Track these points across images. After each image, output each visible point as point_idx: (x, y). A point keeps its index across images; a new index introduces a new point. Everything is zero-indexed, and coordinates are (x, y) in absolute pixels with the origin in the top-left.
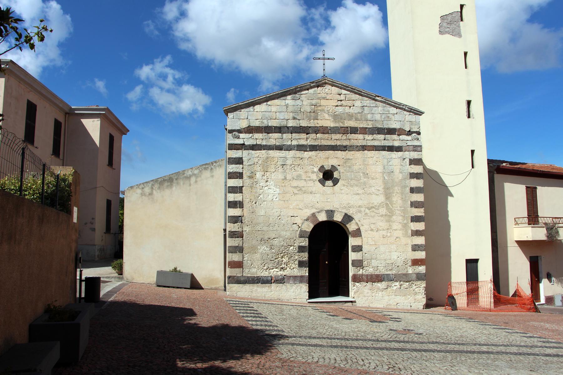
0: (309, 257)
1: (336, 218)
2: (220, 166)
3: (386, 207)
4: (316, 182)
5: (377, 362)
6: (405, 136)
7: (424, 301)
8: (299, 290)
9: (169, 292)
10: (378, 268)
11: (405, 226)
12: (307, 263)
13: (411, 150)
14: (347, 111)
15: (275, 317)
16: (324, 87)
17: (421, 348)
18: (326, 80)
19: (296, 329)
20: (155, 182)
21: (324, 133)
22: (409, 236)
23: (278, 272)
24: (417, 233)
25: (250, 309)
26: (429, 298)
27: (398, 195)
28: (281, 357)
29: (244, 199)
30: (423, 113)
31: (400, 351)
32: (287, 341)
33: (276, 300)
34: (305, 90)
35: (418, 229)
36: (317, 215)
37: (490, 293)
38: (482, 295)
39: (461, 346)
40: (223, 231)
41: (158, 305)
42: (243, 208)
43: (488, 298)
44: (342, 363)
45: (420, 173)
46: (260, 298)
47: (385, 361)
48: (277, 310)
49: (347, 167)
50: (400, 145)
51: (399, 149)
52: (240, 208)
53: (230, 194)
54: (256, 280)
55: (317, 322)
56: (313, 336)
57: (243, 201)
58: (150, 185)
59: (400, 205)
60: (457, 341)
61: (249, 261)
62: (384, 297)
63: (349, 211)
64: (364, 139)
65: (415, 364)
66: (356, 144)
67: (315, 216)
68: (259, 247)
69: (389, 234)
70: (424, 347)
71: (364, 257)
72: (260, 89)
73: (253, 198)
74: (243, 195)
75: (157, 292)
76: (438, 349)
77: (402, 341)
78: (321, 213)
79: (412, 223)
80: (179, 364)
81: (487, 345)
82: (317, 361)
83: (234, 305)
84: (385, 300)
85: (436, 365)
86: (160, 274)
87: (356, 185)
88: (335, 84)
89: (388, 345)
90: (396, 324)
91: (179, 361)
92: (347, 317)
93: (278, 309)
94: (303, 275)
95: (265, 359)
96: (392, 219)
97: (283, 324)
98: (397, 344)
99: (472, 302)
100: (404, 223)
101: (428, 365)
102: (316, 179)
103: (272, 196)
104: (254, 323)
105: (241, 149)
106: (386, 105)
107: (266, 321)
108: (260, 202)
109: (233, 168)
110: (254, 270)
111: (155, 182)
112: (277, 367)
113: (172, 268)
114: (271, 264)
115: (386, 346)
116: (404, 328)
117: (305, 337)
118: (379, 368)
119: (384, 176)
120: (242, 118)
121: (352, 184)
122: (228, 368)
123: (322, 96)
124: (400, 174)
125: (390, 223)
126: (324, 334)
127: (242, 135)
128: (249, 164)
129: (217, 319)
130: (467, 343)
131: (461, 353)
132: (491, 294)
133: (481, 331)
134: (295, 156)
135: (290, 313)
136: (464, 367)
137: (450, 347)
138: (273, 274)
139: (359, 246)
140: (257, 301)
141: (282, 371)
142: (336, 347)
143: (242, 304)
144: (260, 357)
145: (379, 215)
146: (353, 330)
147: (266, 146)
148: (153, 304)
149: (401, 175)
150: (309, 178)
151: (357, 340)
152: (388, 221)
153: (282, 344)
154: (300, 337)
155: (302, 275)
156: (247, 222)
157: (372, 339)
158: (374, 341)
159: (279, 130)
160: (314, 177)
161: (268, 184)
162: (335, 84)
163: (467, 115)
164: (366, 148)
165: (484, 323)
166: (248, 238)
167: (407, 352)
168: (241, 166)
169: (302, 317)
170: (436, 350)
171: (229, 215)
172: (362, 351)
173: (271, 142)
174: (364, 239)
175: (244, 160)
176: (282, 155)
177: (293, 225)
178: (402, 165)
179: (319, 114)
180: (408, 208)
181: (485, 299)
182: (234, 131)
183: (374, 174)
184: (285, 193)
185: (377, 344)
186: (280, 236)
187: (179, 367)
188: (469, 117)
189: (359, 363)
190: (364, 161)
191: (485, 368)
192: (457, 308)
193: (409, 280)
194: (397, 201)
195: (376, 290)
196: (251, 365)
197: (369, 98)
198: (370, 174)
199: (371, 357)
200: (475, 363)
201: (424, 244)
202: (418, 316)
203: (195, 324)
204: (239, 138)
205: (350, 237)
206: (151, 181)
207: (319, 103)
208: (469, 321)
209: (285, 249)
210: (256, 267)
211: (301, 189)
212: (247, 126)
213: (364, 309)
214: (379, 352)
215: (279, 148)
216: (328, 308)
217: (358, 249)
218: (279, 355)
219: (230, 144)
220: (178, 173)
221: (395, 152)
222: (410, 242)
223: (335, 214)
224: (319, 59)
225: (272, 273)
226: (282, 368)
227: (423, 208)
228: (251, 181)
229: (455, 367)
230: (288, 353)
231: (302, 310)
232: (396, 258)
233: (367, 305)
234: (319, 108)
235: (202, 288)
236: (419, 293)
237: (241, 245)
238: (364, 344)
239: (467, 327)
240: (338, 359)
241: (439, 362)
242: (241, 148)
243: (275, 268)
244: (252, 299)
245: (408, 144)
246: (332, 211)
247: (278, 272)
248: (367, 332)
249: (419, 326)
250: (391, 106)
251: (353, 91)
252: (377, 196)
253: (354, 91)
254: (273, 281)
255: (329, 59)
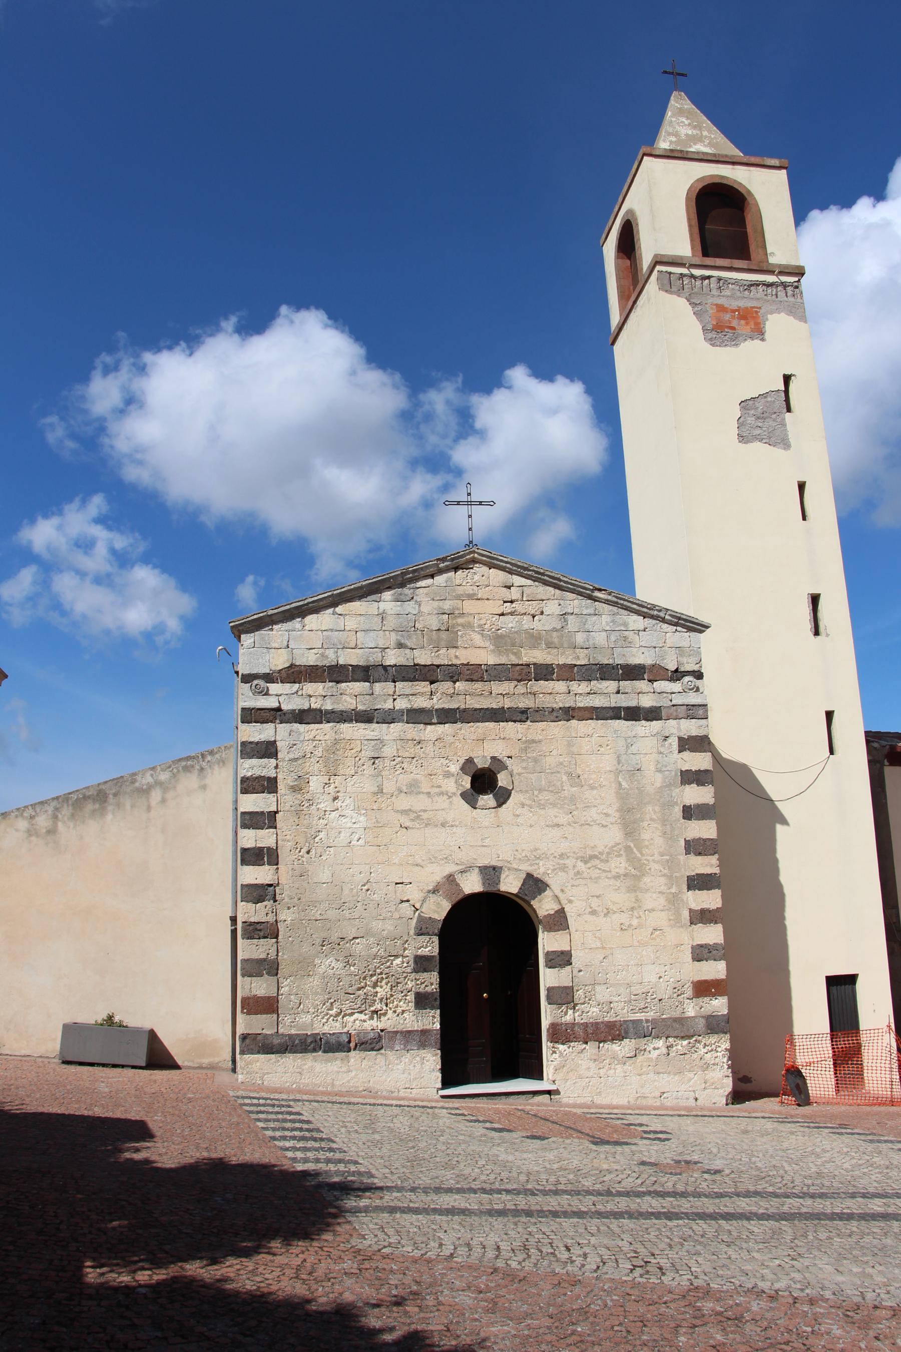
0: (442, 984)
1: (505, 884)
2: (222, 762)
3: (627, 856)
4: (454, 797)
5: (603, 1251)
6: (667, 682)
7: (728, 1085)
8: (418, 1066)
9: (91, 1079)
10: (612, 1005)
11: (674, 900)
12: (436, 999)
13: (681, 716)
14: (526, 627)
15: (354, 1139)
16: (471, 570)
17: (717, 1211)
18: (474, 552)
19: (405, 1170)
20: (63, 801)
21: (472, 681)
22: (685, 924)
23: (365, 1021)
24: (702, 917)
25: (292, 1117)
26: (740, 1076)
27: (655, 825)
28: (360, 1247)
29: (279, 842)
30: (707, 627)
31: (665, 1221)
32: (377, 1201)
33: (361, 1091)
34: (426, 577)
35: (705, 906)
36: (458, 877)
37: (889, 1059)
38: (870, 1064)
39: (818, 1200)
40: (230, 922)
41: (58, 1114)
42: (277, 864)
43: (884, 1072)
44: (515, 1258)
45: (706, 771)
46: (321, 1088)
47: (623, 1249)
48: (359, 1118)
49: (530, 760)
50: (655, 704)
51: (653, 714)
52: (269, 864)
53: (246, 831)
54: (311, 1042)
55: (459, 1150)
56: (445, 1186)
57: (277, 847)
58: (50, 809)
59: (661, 850)
60: (808, 1189)
61: (292, 997)
62: (628, 1078)
63: (536, 867)
64: (569, 693)
65: (700, 1254)
66: (548, 706)
67: (454, 880)
68: (317, 961)
69: (635, 922)
70: (726, 1206)
71: (576, 980)
72: (316, 574)
73: (301, 840)
74: (277, 834)
75: (61, 1079)
76: (761, 1211)
77: (669, 1192)
78: (468, 874)
79: (690, 892)
80: (90, 1276)
81: (883, 1195)
82: (452, 1254)
83: (252, 1108)
84: (631, 1084)
85: (755, 1254)
86: (71, 1031)
87: (551, 804)
88: (496, 562)
89: (633, 1204)
90: (656, 1146)
91: (92, 1267)
92: (535, 1134)
93: (364, 1116)
94: (428, 1027)
95: (317, 1254)
96: (642, 885)
97: (372, 1157)
98: (657, 1201)
99: (845, 1084)
100: (671, 893)
101: (733, 1257)
102: (454, 790)
103: (348, 834)
104: (299, 1155)
105: (271, 722)
106: (620, 610)
107: (331, 1150)
108: (319, 850)
109: (254, 767)
110: (306, 1019)
111: (63, 801)
112: (346, 1273)
113: (101, 1016)
114: (348, 1002)
115: (628, 1206)
116: (675, 1158)
117: (426, 1190)
118: (609, 1268)
119: (620, 779)
120: (276, 645)
121: (542, 802)
122: (219, 1281)
123: (467, 592)
124: (657, 774)
125: (638, 893)
126: (474, 1180)
127: (274, 688)
128: (291, 756)
129: (205, 1146)
130: (833, 1193)
131: (816, 1219)
132: (890, 1061)
133: (869, 1158)
134: (403, 737)
135: (392, 1125)
136: (826, 1259)
137: (790, 1204)
138: (353, 1028)
139: (562, 952)
140: (311, 1097)
141: (359, 1285)
142: (502, 1213)
143: (273, 1106)
144: (304, 1249)
145: (609, 875)
146: (548, 1166)
147: (333, 712)
148: (45, 1110)
149: (659, 776)
150: (437, 790)
151: (556, 1192)
152: (632, 889)
153: (366, 1210)
154: (413, 1190)
155: (425, 1027)
156: (286, 900)
157: (593, 1190)
158: (599, 1193)
159: (364, 673)
160: (450, 785)
161: (340, 804)
162: (496, 562)
163: (813, 630)
164: (575, 714)
165: (876, 1138)
166: (290, 939)
167: (681, 1222)
168: (273, 762)
169: (422, 1136)
170: (756, 1214)
171: (244, 883)
172: (567, 1223)
173: (345, 704)
174: (576, 936)
175: (279, 749)
176: (372, 733)
177: (400, 905)
178: (661, 753)
179: (459, 633)
180: (679, 857)
181: (878, 1075)
182: (255, 676)
183: (593, 776)
184: (379, 825)
185: (607, 1202)
186: (368, 933)
187: (90, 1286)
188: (817, 633)
189: (558, 1256)
190: (570, 745)
191: (879, 1259)
192: (811, 1098)
193: (688, 1034)
194: (652, 839)
195: (607, 1061)
196: (279, 1269)
197: (578, 594)
198: (586, 776)
199: (588, 1238)
200: (852, 1248)
201: (723, 942)
202: (713, 1125)
203: (147, 1161)
204: (267, 694)
205: (540, 931)
206: (53, 799)
207: (458, 609)
208: (838, 1133)
209: (382, 965)
210: (312, 1010)
211: (418, 817)
212: (287, 665)
213: (579, 1111)
214: (611, 1223)
215: (366, 717)
216: (489, 1109)
217: (562, 959)
218: (355, 1241)
219: (245, 708)
220: (118, 781)
221: (643, 722)
222: (686, 938)
223: (503, 876)
224: (458, 503)
225: (350, 1024)
226: (358, 1277)
227: (716, 856)
228: (296, 798)
229: (801, 1260)
230: (379, 1233)
231: (424, 1117)
232: (654, 979)
233: (588, 1100)
234: (460, 621)
235: (176, 1067)
236: (714, 1064)
237: (272, 956)
238: (572, 1203)
239: (832, 1149)
240: (504, 1246)
241: (761, 1246)
242: (271, 718)
243: (358, 1012)
244: (300, 1091)
245: (674, 702)
246: (494, 868)
247: (365, 1021)
248: (583, 1172)
249: (715, 1150)
250: (630, 611)
251: (540, 578)
252: (604, 829)
253: (543, 577)
254: (352, 1045)
255: (480, 503)
